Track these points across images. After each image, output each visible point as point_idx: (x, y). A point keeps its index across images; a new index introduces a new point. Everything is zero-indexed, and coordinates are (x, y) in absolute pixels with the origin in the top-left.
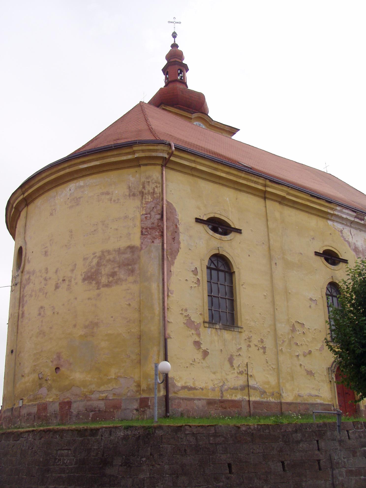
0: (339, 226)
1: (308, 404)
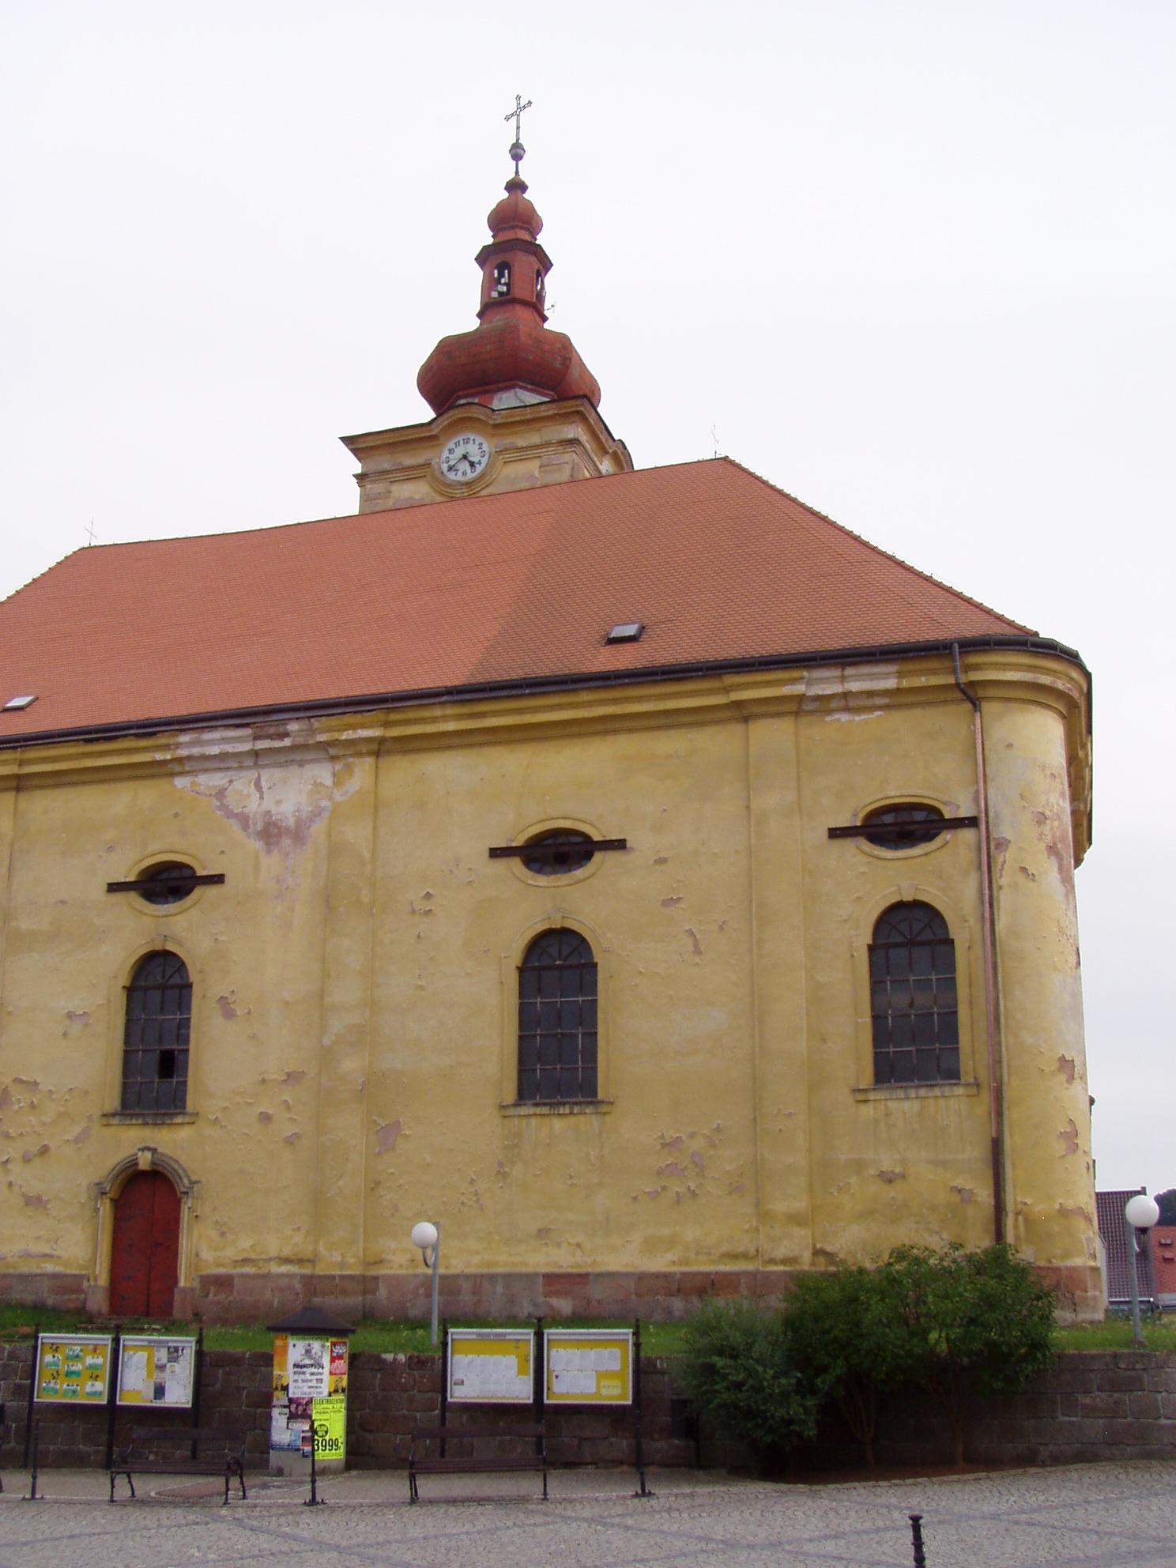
0: (216, 780)
1: (12, 1276)
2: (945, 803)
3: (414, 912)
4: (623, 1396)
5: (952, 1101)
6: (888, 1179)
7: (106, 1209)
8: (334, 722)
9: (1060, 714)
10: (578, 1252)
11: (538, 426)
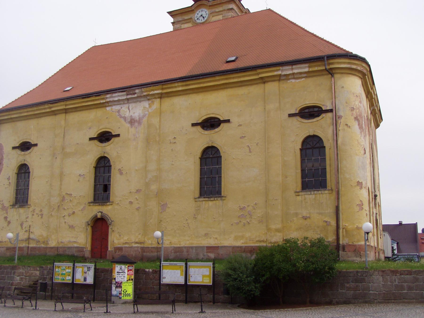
0: (117, 107)
1: (66, 247)
2: (323, 105)
3: (171, 143)
4: (209, 282)
5: (324, 195)
6: (305, 218)
7: (89, 229)
8: (148, 89)
9: (360, 77)
10: (216, 240)
11: (221, 5)
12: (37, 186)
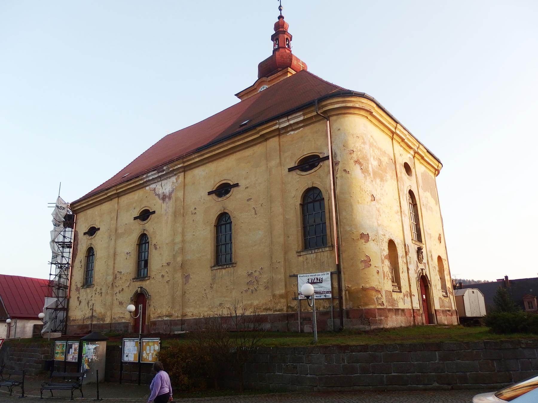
0: (153, 186)
12: (100, 266)
